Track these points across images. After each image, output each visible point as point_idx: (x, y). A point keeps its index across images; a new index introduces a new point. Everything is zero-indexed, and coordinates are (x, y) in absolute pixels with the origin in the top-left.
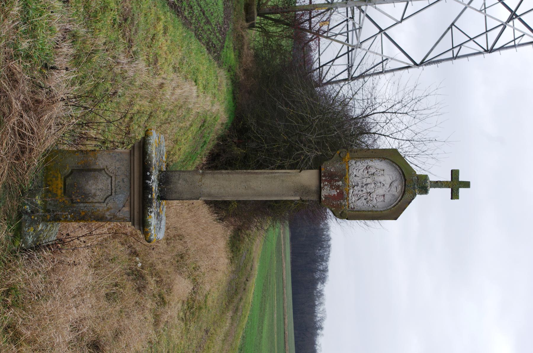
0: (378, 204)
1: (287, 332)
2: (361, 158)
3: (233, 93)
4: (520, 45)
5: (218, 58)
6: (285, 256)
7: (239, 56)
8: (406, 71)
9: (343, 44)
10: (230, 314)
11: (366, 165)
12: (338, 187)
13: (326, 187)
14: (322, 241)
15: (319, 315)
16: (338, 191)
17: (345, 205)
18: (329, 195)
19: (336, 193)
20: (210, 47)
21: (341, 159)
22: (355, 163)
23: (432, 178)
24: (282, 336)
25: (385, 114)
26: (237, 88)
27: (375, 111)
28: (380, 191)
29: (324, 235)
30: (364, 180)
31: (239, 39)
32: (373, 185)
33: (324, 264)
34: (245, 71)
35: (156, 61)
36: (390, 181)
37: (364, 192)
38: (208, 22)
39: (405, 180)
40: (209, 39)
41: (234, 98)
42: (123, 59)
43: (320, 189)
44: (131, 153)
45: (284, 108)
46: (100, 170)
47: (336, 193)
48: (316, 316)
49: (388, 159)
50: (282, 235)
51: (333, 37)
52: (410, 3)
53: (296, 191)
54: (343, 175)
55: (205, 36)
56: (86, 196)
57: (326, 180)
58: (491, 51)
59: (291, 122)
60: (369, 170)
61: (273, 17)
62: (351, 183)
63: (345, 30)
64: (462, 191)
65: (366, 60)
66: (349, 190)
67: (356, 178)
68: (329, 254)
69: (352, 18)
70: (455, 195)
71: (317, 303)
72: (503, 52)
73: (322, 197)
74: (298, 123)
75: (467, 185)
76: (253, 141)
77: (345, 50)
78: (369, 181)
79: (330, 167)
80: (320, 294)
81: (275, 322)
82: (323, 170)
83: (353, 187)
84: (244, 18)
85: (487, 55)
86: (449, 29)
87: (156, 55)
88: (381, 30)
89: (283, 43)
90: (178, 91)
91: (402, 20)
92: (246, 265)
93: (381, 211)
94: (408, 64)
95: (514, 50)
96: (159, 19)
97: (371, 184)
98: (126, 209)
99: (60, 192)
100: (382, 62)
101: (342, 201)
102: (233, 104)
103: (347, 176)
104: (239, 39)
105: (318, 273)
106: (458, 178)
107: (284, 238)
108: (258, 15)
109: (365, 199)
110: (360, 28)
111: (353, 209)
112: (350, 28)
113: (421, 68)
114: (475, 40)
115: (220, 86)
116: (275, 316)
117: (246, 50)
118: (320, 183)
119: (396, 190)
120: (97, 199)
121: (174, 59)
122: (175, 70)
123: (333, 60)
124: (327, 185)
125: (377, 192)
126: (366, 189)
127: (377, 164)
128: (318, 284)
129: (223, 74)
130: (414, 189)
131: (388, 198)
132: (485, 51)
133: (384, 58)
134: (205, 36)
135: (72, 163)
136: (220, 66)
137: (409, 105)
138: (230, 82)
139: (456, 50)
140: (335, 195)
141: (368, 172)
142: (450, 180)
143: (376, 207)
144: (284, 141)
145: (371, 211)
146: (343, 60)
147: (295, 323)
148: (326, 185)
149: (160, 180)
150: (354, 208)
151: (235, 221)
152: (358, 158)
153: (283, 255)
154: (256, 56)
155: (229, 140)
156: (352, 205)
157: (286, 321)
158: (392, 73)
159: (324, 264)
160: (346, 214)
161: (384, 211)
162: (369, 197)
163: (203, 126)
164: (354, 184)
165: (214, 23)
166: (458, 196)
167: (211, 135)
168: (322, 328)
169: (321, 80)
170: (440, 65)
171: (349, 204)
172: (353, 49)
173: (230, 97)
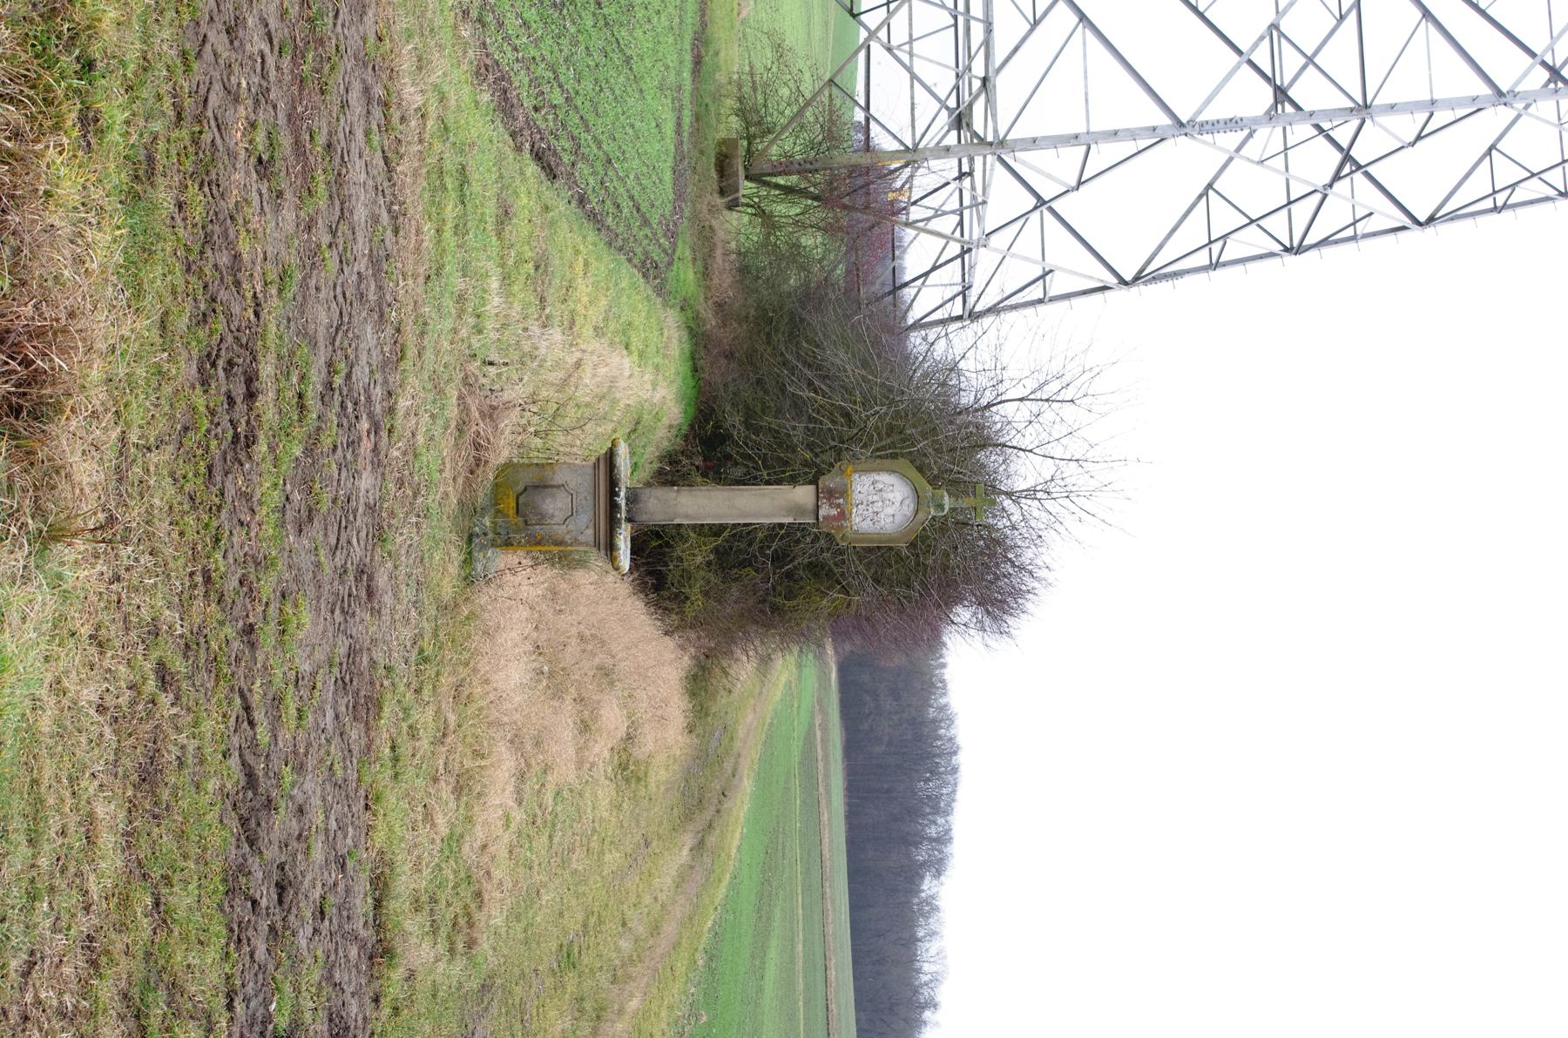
1: (833, 1007)
3: (693, 358)
4: (1365, 236)
5: (659, 290)
6: (828, 792)
7: (706, 274)
8: (1098, 296)
9: (948, 238)
10: (688, 840)
12: (839, 506)
14: (935, 755)
15: (926, 967)
20: (650, 270)
21: (842, 471)
24: (821, 1014)
25: (1055, 405)
26: (700, 342)
27: (1004, 398)
28: (890, 511)
29: (940, 738)
31: (705, 237)
33: (941, 821)
34: (719, 306)
35: (572, 323)
38: (646, 222)
40: (646, 253)
41: (695, 370)
42: (535, 329)
44: (596, 466)
45: (807, 394)
46: (558, 487)
48: (919, 971)
50: (818, 734)
51: (921, 225)
52: (1093, 147)
53: (789, 512)
54: (844, 492)
55: (639, 250)
56: (542, 518)
61: (781, 181)
63: (954, 204)
65: (998, 273)
68: (954, 791)
69: (970, 174)
71: (921, 934)
72: (1327, 251)
74: (834, 422)
76: (736, 464)
77: (954, 249)
79: (827, 481)
80: (931, 907)
81: (800, 964)
84: (716, 187)
85: (1290, 259)
86: (1200, 197)
87: (572, 312)
88: (1041, 202)
89: (807, 241)
90: (602, 371)
91: (1080, 183)
92: (720, 760)
95: (1352, 245)
96: (577, 252)
98: (590, 532)
99: (512, 512)
100: (1043, 277)
102: (692, 383)
104: (705, 237)
105: (925, 846)
107: (824, 741)
108: (747, 178)
110: (984, 202)
112: (966, 202)
113: (1134, 290)
114: (1261, 223)
115: (666, 347)
116: (800, 947)
117: (719, 260)
120: (556, 520)
121: (595, 314)
122: (598, 331)
123: (926, 274)
128: (922, 878)
129: (672, 318)
131: (898, 519)
132: (1286, 250)
134: (639, 250)
135: (526, 478)
136: (665, 304)
137: (1077, 383)
138: (685, 336)
139: (1216, 247)
144: (806, 464)
146: (952, 272)
147: (857, 989)
149: (627, 499)
151: (699, 638)
153: (821, 789)
154: (744, 270)
155: (685, 461)
157: (832, 974)
158: (1066, 303)
159: (941, 821)
163: (635, 430)
165: (654, 222)
167: (650, 449)
168: (934, 1005)
170: (1179, 282)
173: (685, 368)
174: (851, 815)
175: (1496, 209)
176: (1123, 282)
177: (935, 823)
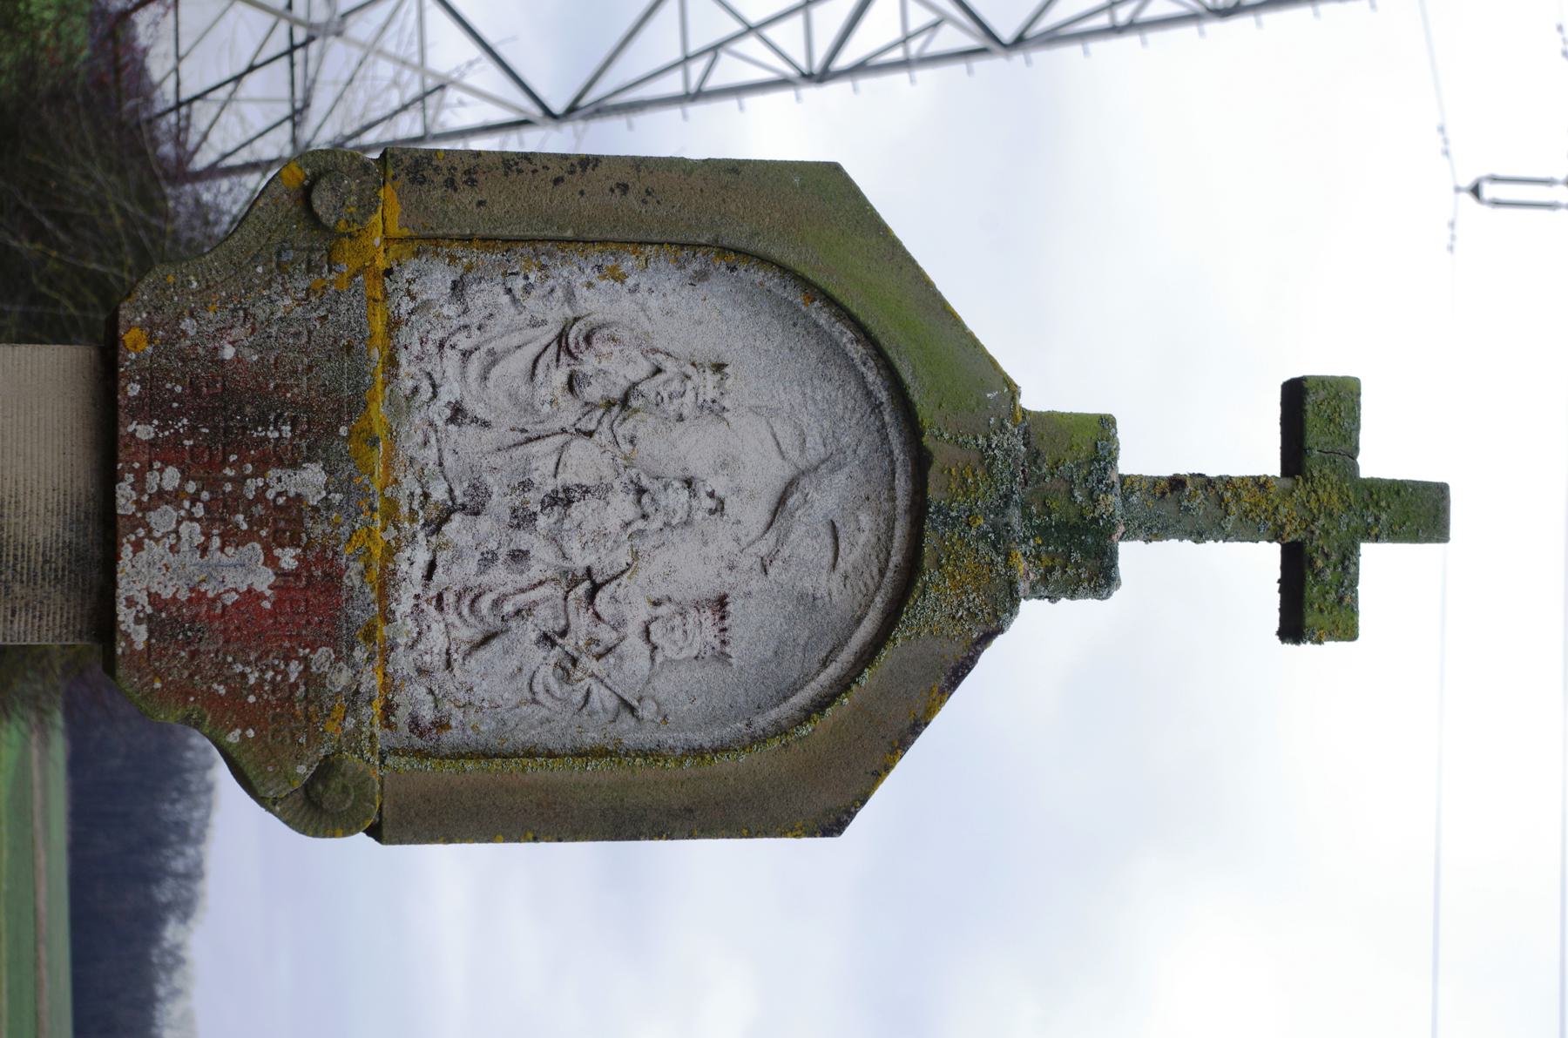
0: (664, 687)
2: (510, 242)
11: (556, 314)
12: (286, 521)
13: (164, 519)
16: (288, 558)
17: (354, 696)
18: (198, 597)
19: (263, 581)
22: (458, 288)
23: (1139, 458)
28: (689, 565)
30: (541, 457)
32: (622, 506)
33: (190, 851)
36: (777, 472)
37: (535, 572)
39: (921, 461)
43: (103, 533)
47: (263, 581)
49: (764, 261)
57: (162, 451)
58: (823, 76)
59: (57, 303)
60: (589, 363)
62: (409, 484)
64: (1382, 567)
66: (390, 552)
67: (466, 438)
68: (208, 815)
70: (1313, 604)
71: (161, 991)
72: (866, 83)
73: (125, 615)
74: (82, 307)
75: (1419, 512)
77: (279, 42)
78: (585, 462)
80: (176, 960)
82: (135, 344)
83: (436, 526)
85: (810, 92)
93: (698, 752)
94: (521, 111)
97: (602, 491)
101: (323, 655)
103: (379, 412)
105: (170, 882)
106: (1355, 468)
109: (547, 639)
111: (427, 740)
114: (769, 32)
118: (108, 478)
119: (830, 555)
123: (237, 79)
124: (175, 498)
125: (651, 568)
126: (554, 539)
127: (660, 312)
130: (1000, 539)
133: (431, 83)
139: (697, 68)
140: (252, 595)
141: (572, 384)
142: (1271, 466)
143: (648, 711)
145: (600, 753)
146: (271, 85)
148: (161, 496)
150: (441, 725)
152: (488, 242)
153: (38, 824)
156: (417, 700)
159: (190, 851)
160: (362, 783)
161: (720, 749)
162: (582, 623)
164: (439, 493)
166: (1353, 611)
169: (184, 158)
171: (390, 685)
172: (310, 39)
174: (77, 847)
175: (1115, 30)
176: (548, 113)
177: (182, 854)
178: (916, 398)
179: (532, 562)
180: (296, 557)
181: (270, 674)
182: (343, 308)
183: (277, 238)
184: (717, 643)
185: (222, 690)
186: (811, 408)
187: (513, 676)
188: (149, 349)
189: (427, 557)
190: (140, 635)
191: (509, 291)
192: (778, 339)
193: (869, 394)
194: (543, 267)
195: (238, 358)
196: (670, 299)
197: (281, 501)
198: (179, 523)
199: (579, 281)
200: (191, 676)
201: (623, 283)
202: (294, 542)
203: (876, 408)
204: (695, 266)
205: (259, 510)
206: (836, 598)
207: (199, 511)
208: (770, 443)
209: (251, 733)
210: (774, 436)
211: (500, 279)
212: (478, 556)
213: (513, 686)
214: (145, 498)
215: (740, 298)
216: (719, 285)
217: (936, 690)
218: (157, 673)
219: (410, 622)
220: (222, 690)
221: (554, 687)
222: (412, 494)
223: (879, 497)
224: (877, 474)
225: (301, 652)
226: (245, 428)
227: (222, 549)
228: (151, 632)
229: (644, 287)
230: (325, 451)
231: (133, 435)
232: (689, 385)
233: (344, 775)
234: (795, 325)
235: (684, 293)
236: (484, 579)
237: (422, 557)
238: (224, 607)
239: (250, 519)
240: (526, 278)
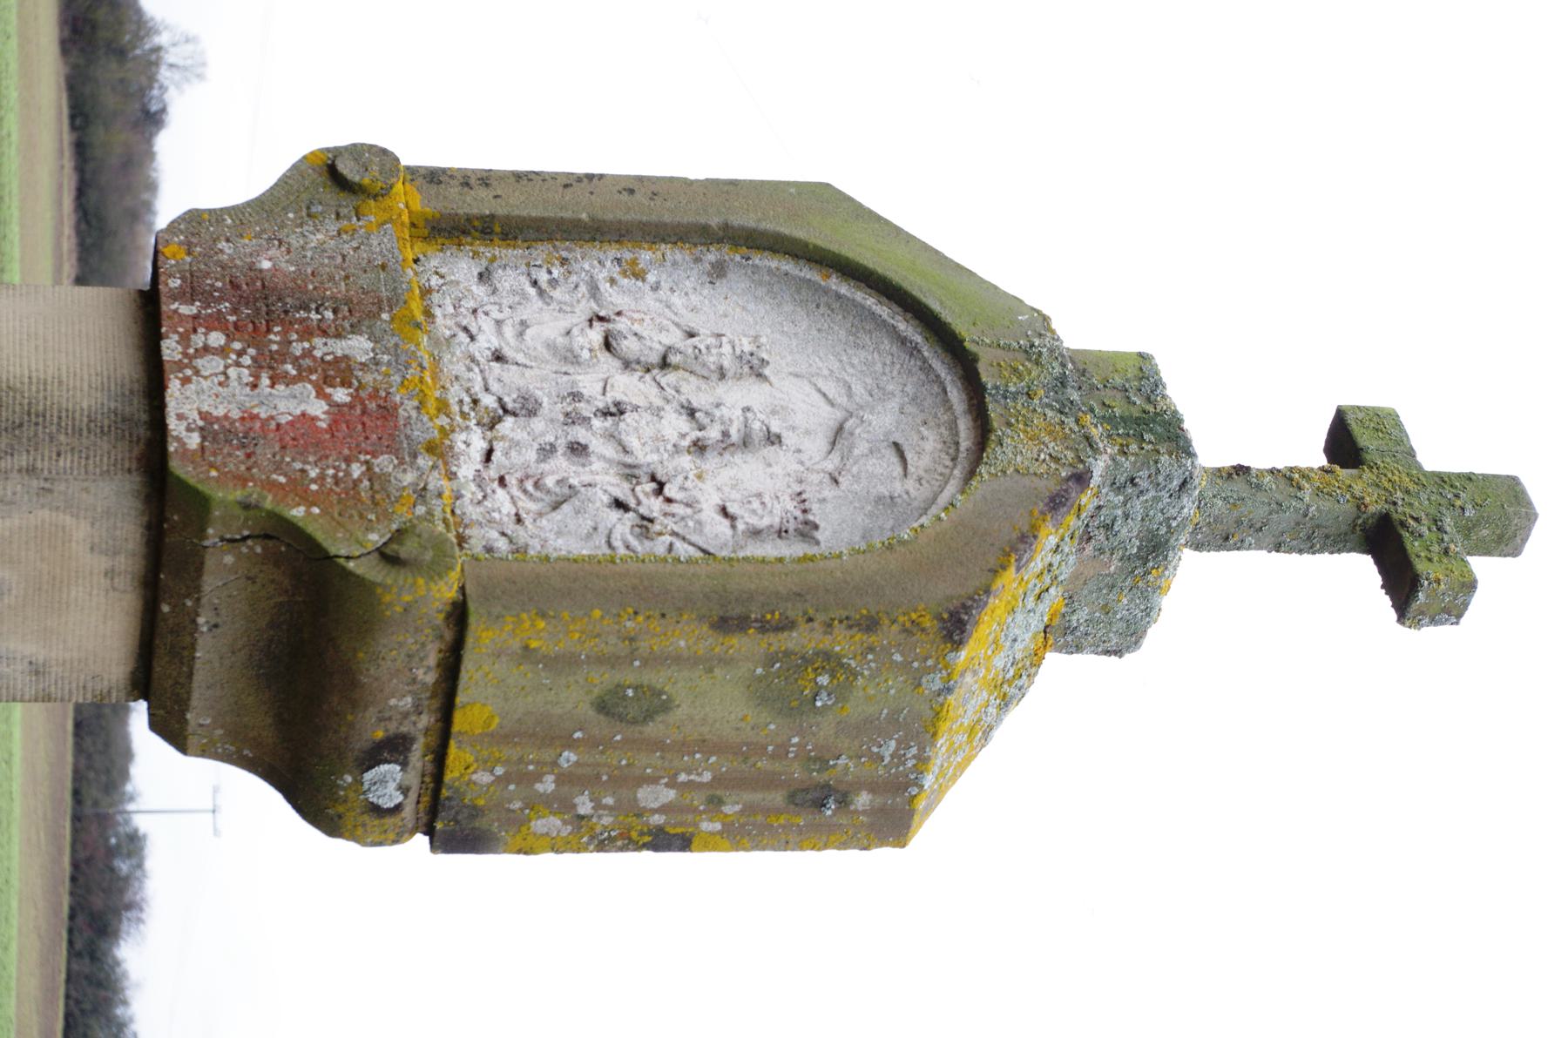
16: (341, 395)
22: (483, 277)
36: (828, 416)
47: (318, 408)
178: (949, 320)
179: (593, 458)
180: (350, 395)
181: (331, 472)
182: (375, 243)
183: (304, 196)
184: (798, 513)
185: (282, 479)
186: (851, 371)
187: (589, 536)
188: (188, 259)
189: (485, 445)
190: (194, 441)
191: (535, 283)
192: (805, 325)
193: (903, 341)
194: (564, 262)
195: (275, 268)
196: (693, 297)
197: (329, 358)
198: (226, 367)
199: (601, 276)
200: (249, 469)
201: (644, 280)
202: (345, 383)
203: (914, 351)
204: (712, 257)
205: (307, 362)
206: (913, 493)
207: (246, 360)
208: (817, 397)
209: (316, 510)
210: (819, 391)
211: (523, 268)
212: (536, 446)
213: (591, 544)
214: (191, 351)
215: (760, 292)
216: (737, 280)
217: (1036, 513)
218: (212, 466)
219: (473, 487)
220: (282, 479)
221: (634, 543)
222: (461, 401)
223: (936, 416)
224: (929, 401)
225: (362, 457)
226: (286, 312)
227: (272, 386)
228: (204, 438)
229: (665, 286)
230: (369, 327)
231: (176, 311)
232: (724, 339)
233: (419, 536)
234: (818, 306)
235: (705, 292)
236: (545, 467)
237: (479, 444)
238: (278, 425)
239: (299, 368)
240: (550, 272)
